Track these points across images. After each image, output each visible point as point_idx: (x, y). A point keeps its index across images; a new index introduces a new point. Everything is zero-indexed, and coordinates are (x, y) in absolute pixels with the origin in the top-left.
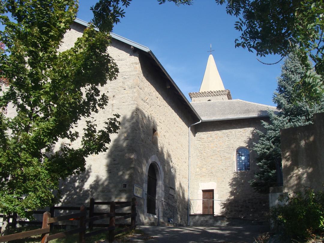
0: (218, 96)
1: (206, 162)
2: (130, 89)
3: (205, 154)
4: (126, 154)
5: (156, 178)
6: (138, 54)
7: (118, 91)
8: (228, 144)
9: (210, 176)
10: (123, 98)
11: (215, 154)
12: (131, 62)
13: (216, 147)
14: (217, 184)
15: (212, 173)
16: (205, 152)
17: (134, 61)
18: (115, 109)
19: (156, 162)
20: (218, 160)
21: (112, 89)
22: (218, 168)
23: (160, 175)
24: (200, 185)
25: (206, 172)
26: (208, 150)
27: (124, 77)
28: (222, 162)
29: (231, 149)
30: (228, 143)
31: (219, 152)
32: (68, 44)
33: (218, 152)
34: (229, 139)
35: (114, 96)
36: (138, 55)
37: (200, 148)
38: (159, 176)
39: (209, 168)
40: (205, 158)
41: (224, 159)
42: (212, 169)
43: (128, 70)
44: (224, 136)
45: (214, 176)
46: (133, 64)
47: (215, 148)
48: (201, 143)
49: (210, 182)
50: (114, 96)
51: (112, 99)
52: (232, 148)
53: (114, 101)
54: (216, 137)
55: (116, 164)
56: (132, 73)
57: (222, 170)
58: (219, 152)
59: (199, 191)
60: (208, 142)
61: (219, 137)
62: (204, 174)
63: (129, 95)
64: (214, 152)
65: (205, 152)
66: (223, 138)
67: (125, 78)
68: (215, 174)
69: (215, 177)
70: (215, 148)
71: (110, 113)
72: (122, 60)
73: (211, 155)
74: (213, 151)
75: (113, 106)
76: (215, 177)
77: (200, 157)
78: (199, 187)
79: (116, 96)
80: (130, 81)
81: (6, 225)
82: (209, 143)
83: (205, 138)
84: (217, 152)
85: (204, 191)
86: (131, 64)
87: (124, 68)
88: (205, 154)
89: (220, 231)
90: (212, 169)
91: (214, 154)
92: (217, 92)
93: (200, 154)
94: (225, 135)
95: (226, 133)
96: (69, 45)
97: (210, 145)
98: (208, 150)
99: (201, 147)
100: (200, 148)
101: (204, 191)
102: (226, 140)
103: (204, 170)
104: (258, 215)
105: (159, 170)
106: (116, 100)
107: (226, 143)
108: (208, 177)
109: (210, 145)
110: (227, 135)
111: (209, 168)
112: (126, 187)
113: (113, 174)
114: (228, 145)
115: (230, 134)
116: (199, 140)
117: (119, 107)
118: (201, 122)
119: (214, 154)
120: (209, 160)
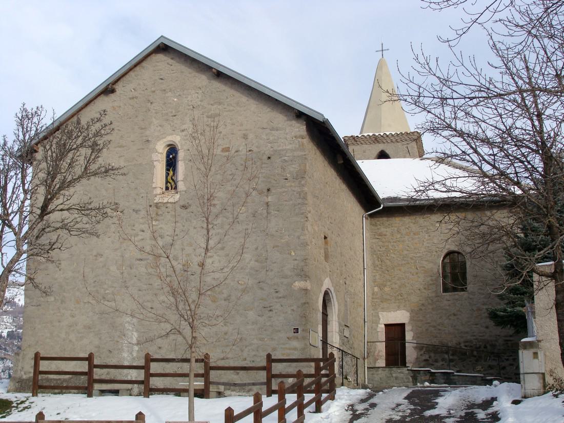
0: (399, 142)
1: (391, 275)
2: (295, 180)
3: (388, 263)
4: (295, 282)
5: (327, 312)
6: (305, 121)
7: (275, 182)
8: (428, 245)
9: (398, 301)
10: (284, 194)
11: (406, 262)
12: (293, 134)
13: (408, 251)
14: (410, 313)
15: (401, 296)
16: (387, 259)
17: (298, 134)
18: (272, 211)
19: (329, 289)
20: (411, 273)
21: (264, 177)
22: (411, 288)
23: (333, 307)
24: (380, 315)
25: (391, 294)
26: (393, 255)
27: (283, 158)
28: (419, 277)
29: (435, 255)
30: (427, 243)
31: (413, 259)
32: (178, 93)
33: (411, 258)
34: (430, 236)
35: (268, 190)
36: (305, 123)
37: (379, 251)
38: (332, 309)
39: (397, 286)
40: (388, 269)
41: (422, 272)
42: (402, 289)
43: (289, 147)
44: (422, 232)
45: (405, 301)
46: (297, 138)
47: (405, 252)
48: (381, 243)
49: (398, 311)
50: (268, 190)
51: (265, 193)
52: (435, 253)
53: (269, 197)
54: (407, 233)
55: (280, 298)
56: (296, 154)
57: (419, 290)
58: (413, 259)
59: (379, 326)
60: (394, 242)
61: (412, 234)
62: (388, 297)
63: (294, 189)
64: (405, 259)
65: (387, 259)
66: (419, 234)
67: (284, 160)
68: (407, 298)
69: (407, 301)
70: (405, 252)
71: (264, 216)
72: (277, 130)
73: (399, 265)
74: (402, 257)
75: (268, 206)
76: (407, 301)
77: (380, 268)
78: (380, 319)
79: (273, 191)
80: (293, 166)
81: (407, 395)
82: (395, 244)
83: (387, 233)
84: (409, 259)
85: (386, 325)
86: (294, 138)
87: (282, 144)
88: (388, 263)
89: (58, 375)
90: (402, 289)
91: (404, 262)
92: (396, 135)
93: (380, 262)
94: (423, 229)
95: (425, 226)
96: (179, 95)
97: (396, 246)
98: (393, 255)
99: (381, 250)
100: (379, 251)
101: (386, 325)
102: (425, 238)
103: (387, 289)
104: (482, 368)
105: (332, 299)
106: (273, 195)
107: (425, 244)
108: (395, 303)
109: (396, 246)
110: (426, 229)
111: (397, 286)
112: (298, 332)
113: (276, 313)
114: (428, 247)
115: (431, 228)
116: (377, 237)
117: (278, 208)
118: (383, 207)
119: (404, 262)
120: (395, 273)
